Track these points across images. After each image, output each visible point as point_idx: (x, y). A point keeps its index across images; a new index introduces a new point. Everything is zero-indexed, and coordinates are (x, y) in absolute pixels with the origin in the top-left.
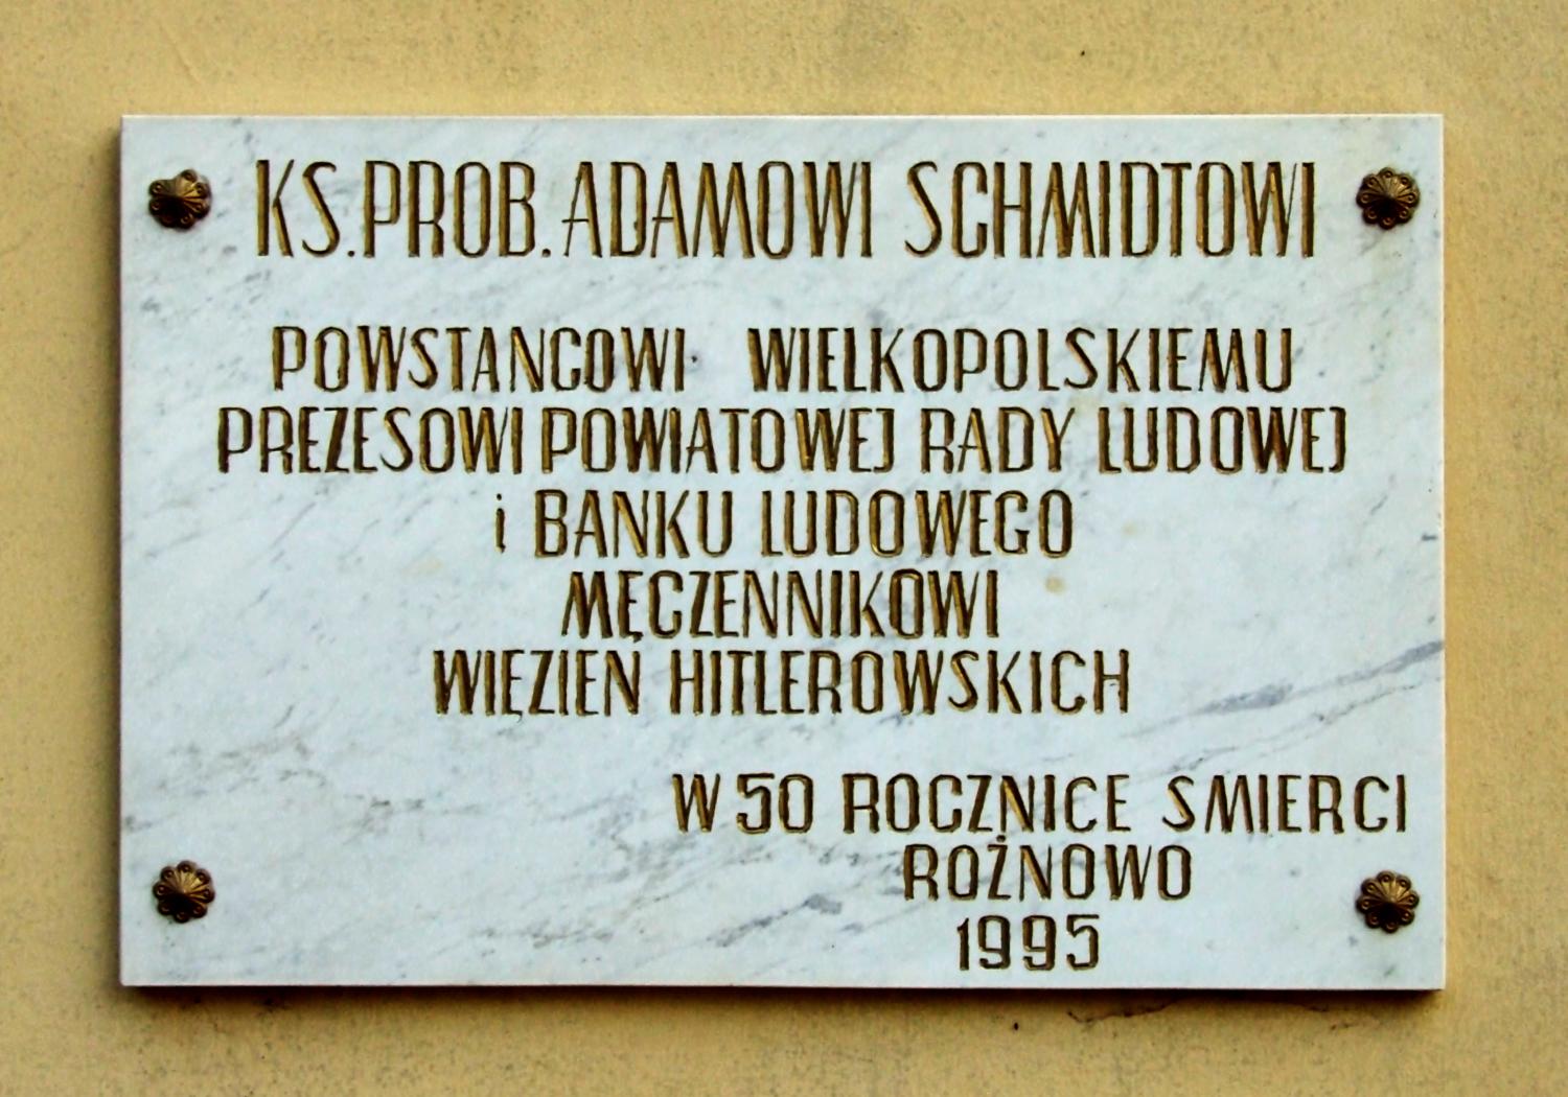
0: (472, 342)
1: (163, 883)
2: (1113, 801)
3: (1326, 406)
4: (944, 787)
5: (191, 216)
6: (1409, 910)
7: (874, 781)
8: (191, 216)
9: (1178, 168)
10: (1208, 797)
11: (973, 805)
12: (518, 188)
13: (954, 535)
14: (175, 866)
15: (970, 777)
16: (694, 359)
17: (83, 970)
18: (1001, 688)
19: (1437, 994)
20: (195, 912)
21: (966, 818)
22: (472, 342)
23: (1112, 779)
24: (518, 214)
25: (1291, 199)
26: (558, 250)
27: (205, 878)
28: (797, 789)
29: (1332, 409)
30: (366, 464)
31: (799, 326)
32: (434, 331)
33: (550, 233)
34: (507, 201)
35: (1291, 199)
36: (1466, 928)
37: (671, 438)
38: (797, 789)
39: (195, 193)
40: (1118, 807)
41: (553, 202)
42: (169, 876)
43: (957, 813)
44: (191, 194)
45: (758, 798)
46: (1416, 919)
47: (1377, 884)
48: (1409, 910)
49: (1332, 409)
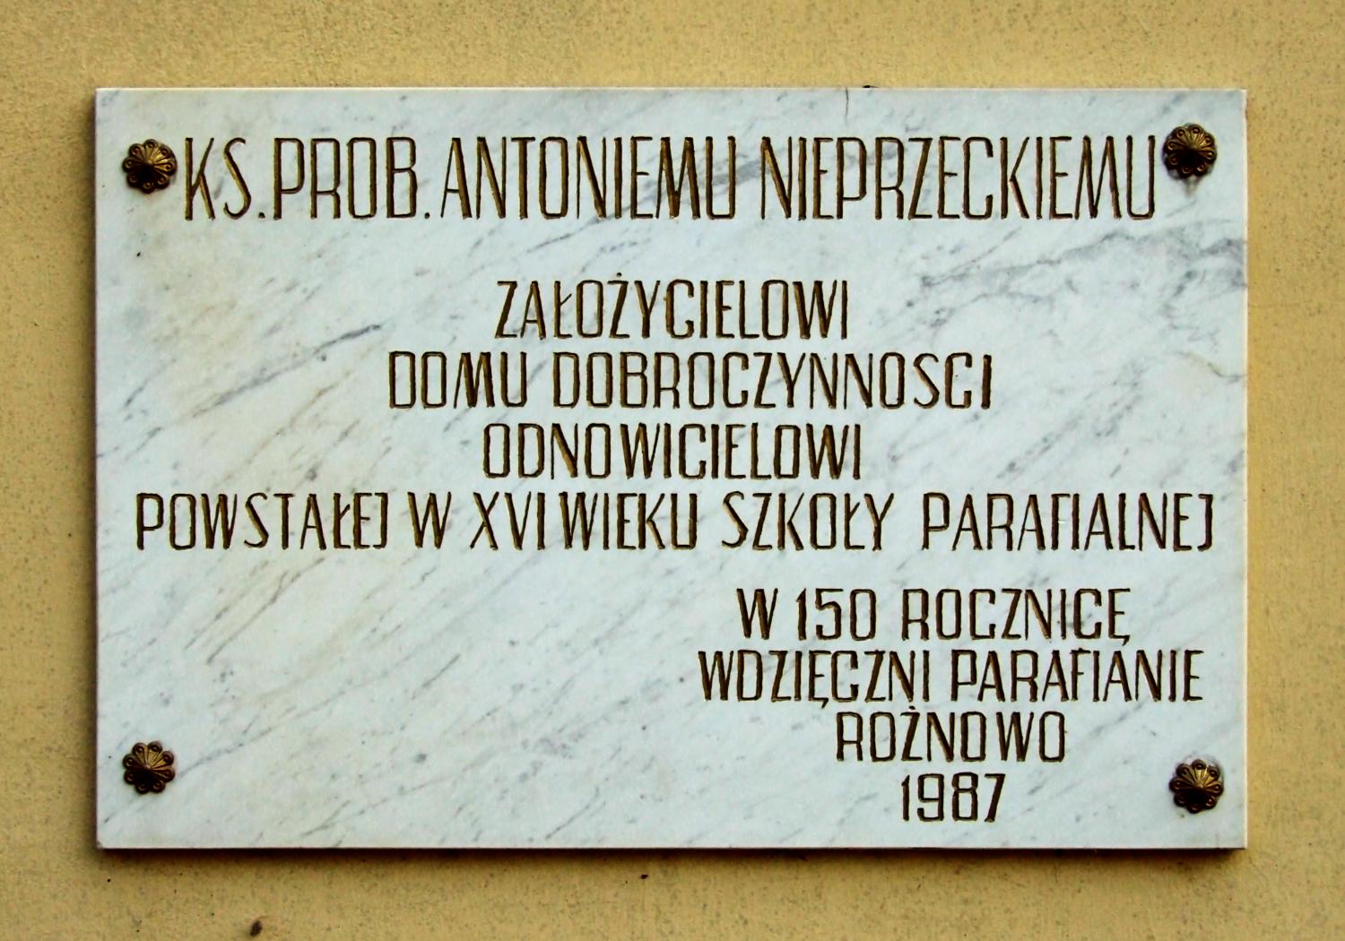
1: (133, 757)
4: (982, 599)
5: (165, 176)
7: (925, 594)
8: (165, 176)
9: (524, 142)
11: (1017, 609)
12: (402, 160)
13: (587, 535)
14: (147, 744)
15: (1005, 590)
17: (66, 832)
19: (1238, 855)
20: (155, 788)
21: (863, 692)
23: (1112, 592)
24: (402, 181)
25: (479, 197)
26: (435, 212)
27: (169, 759)
28: (863, 601)
30: (725, 331)
33: (429, 197)
34: (392, 170)
35: (479, 197)
36: (1263, 811)
38: (863, 601)
39: (1204, 143)
41: (433, 170)
42: (140, 752)
43: (855, 689)
45: (830, 612)
46: (1217, 805)
47: (1191, 770)
48: (1214, 798)
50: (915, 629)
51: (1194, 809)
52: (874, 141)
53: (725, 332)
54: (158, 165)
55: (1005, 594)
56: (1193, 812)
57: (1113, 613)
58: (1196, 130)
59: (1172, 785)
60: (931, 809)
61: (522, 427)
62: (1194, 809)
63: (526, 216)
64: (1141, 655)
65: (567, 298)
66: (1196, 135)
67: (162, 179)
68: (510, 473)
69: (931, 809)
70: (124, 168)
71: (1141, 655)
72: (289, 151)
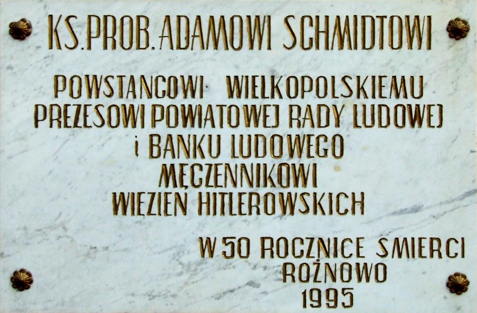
4: (297, 242)
8: (465, 32)
15: (307, 238)
16: (207, 87)
23: (358, 239)
28: (244, 242)
33: (154, 41)
34: (139, 30)
38: (244, 242)
41: (155, 31)
45: (230, 246)
50: (268, 253)
51: (459, 293)
52: (87, 17)
53: (383, 95)
54: (462, 28)
55: (307, 240)
56: (459, 294)
57: (358, 247)
58: (458, 20)
59: (448, 285)
60: (332, 304)
61: (257, 136)
62: (459, 293)
63: (318, 49)
64: (366, 264)
65: (366, 80)
66: (459, 22)
67: (464, 34)
68: (251, 156)
69: (332, 304)
70: (447, 30)
71: (366, 264)
72: (94, 20)
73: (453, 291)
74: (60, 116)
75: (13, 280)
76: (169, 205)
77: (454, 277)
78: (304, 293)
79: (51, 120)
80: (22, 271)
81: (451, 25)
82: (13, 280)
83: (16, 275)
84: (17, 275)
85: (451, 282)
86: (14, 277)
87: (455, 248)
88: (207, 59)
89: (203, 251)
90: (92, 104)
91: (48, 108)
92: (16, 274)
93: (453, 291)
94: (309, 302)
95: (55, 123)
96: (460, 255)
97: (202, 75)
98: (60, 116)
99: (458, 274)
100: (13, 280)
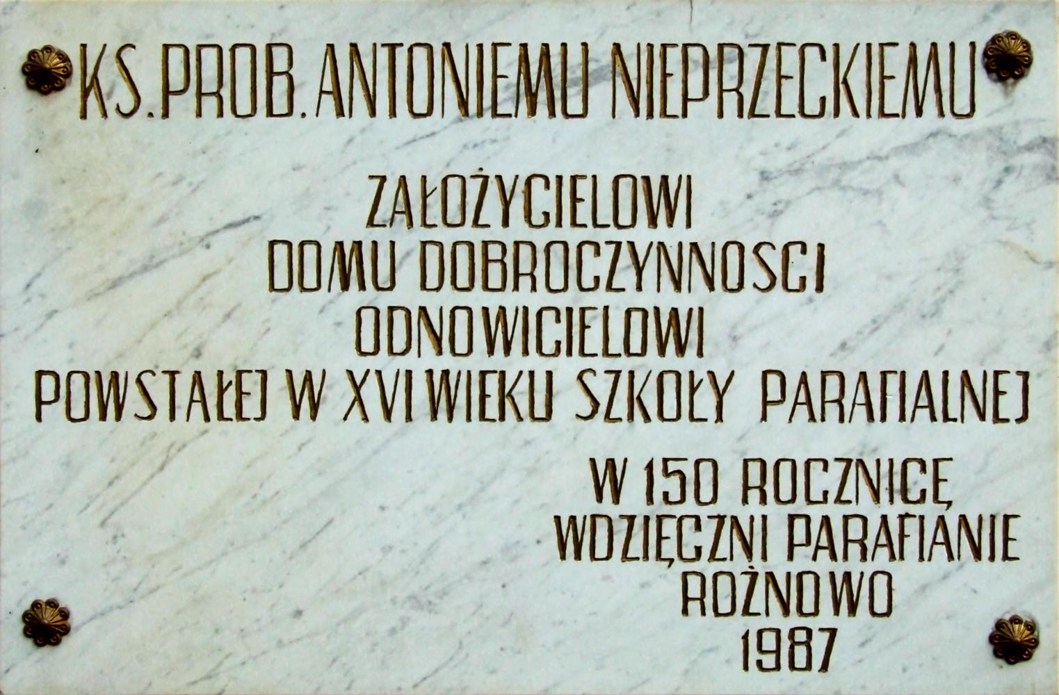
0: (184, 384)
2: (937, 481)
3: (1013, 370)
6: (1023, 68)
10: (925, 102)
16: (671, 247)
18: (842, 87)
22: (184, 384)
24: (280, 84)
25: (351, 99)
29: (1019, 373)
31: (346, 119)
32: (594, 372)
33: (306, 98)
35: (351, 99)
37: (339, 263)
39: (1021, 49)
40: (941, 485)
44: (56, 619)
48: (1023, 68)
49: (1019, 373)
51: (1012, 660)
56: (1010, 663)
59: (992, 639)
62: (1012, 660)
73: (1000, 654)
74: (221, 83)
75: (27, 620)
76: (579, 205)
77: (1009, 625)
78: (745, 637)
79: (200, 94)
80: (52, 604)
81: (996, 44)
82: (27, 620)
83: (35, 609)
84: (38, 612)
85: (999, 633)
86: (32, 613)
87: (803, 265)
88: (460, 581)
89: (562, 546)
90: (857, 42)
91: (713, 53)
92: (38, 608)
93: (1000, 654)
94: (754, 655)
95: (210, 104)
96: (811, 283)
97: (646, 174)
98: (221, 83)
99: (1017, 619)
100: (28, 618)
